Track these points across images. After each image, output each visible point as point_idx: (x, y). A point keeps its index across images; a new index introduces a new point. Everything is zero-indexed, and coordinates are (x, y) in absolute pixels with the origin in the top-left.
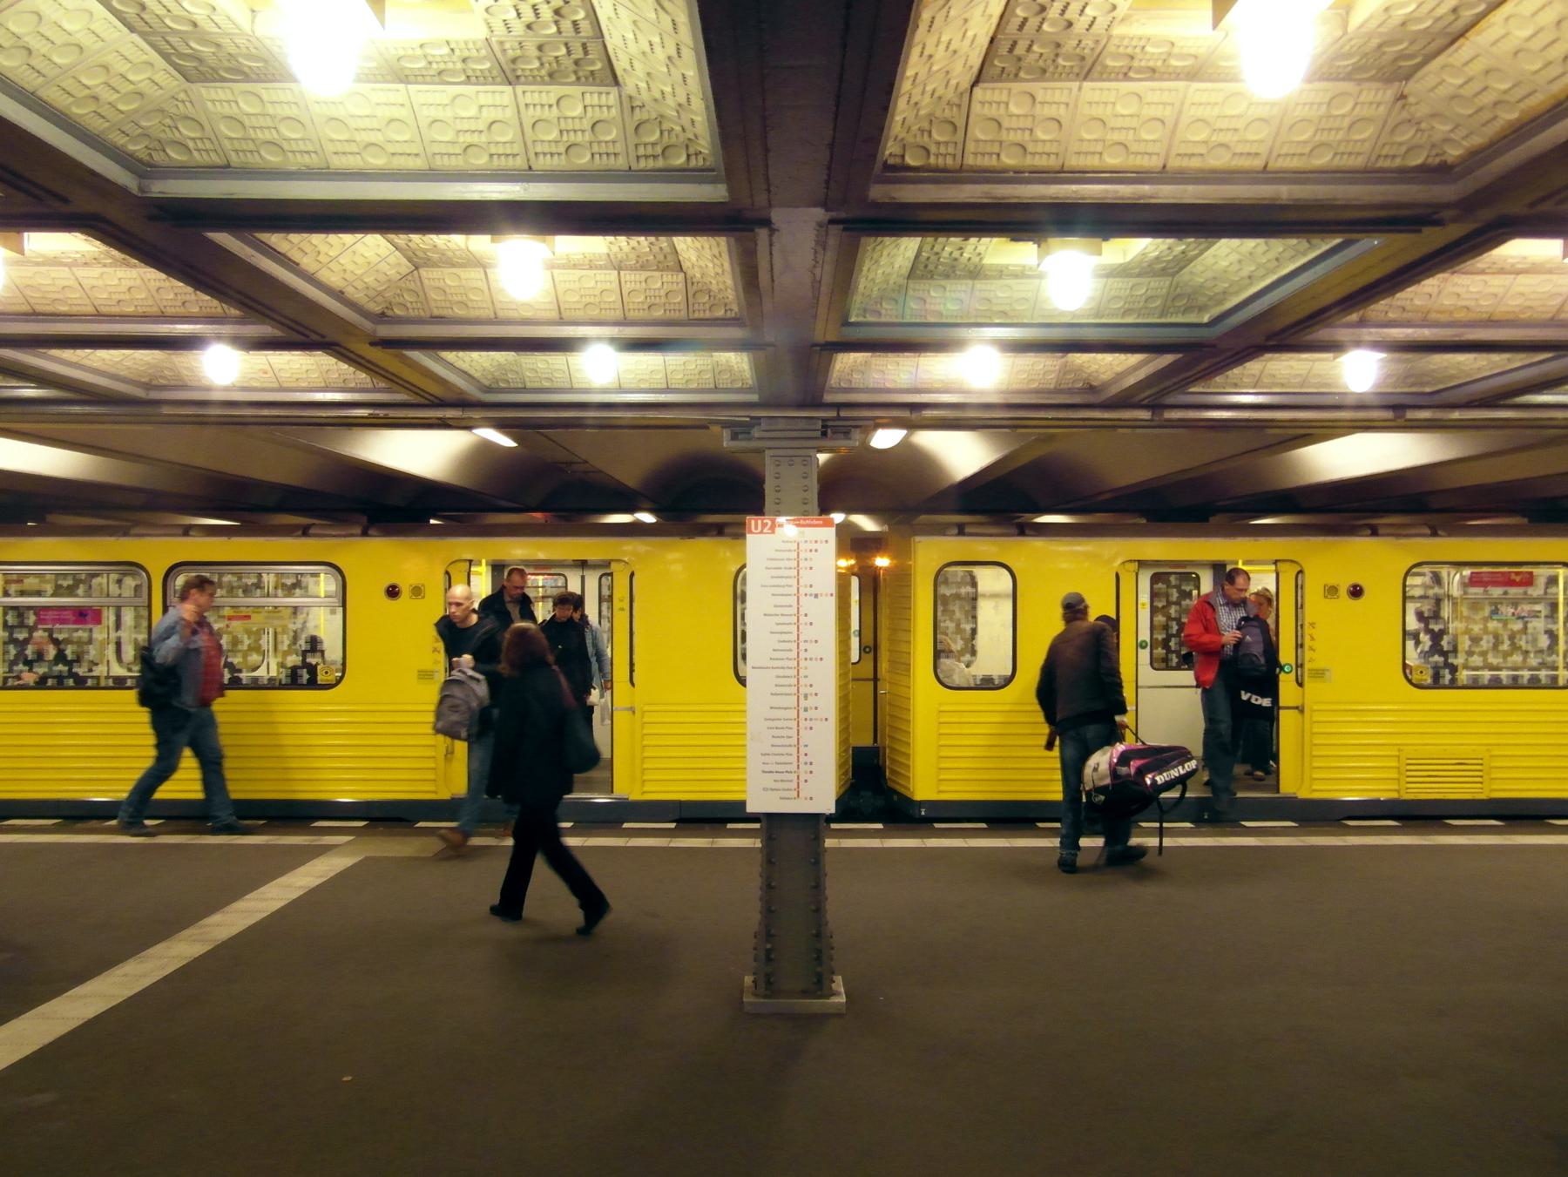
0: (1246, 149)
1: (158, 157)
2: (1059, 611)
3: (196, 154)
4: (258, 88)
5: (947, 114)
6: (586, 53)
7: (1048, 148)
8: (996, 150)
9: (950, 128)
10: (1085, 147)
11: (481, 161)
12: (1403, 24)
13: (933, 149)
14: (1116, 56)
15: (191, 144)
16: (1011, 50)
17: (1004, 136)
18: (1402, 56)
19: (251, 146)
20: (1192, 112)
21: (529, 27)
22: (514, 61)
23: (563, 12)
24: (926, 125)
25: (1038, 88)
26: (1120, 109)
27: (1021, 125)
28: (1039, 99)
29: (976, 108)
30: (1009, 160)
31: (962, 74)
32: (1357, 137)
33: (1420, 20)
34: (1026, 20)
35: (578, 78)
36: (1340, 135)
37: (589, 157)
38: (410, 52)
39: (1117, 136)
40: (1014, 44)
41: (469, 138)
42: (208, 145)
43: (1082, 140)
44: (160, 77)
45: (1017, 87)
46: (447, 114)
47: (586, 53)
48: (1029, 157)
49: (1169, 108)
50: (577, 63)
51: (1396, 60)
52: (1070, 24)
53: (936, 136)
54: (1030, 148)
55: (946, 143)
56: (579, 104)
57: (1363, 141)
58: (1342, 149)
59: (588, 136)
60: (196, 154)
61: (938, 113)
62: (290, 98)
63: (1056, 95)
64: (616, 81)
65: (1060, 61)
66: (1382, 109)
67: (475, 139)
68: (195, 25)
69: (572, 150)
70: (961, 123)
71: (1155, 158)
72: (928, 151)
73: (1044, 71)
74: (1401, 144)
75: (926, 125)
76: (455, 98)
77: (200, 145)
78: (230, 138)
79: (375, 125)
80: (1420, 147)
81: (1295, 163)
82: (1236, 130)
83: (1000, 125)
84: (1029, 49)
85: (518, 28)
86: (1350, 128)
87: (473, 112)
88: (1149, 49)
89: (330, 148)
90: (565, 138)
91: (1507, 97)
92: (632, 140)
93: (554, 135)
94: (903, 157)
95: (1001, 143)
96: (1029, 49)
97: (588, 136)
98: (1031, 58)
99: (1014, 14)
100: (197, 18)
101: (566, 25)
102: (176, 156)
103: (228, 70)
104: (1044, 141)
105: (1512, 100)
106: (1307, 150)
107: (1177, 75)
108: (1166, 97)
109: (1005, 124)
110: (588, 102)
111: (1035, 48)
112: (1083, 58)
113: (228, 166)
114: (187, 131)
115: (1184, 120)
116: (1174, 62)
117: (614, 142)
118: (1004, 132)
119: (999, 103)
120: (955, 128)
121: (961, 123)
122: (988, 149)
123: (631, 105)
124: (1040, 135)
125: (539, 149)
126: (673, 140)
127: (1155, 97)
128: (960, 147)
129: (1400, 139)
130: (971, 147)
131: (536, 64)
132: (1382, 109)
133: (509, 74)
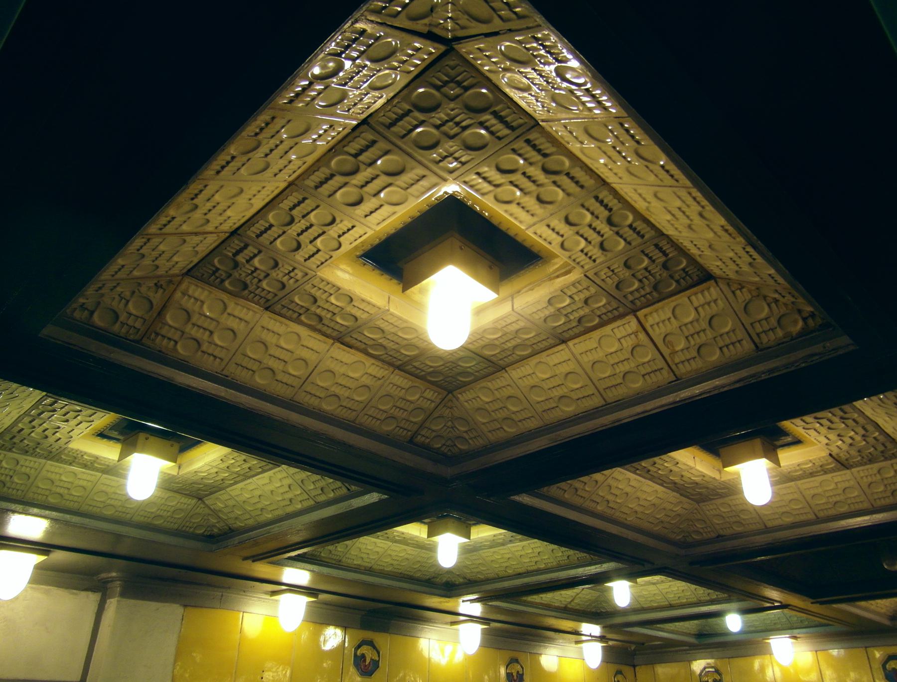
10: (245, 362)
13: (122, 318)
14: (67, 455)
16: (11, 439)
17: (188, 328)
25: (22, 458)
26: (63, 478)
27: (205, 325)
28: (229, 310)
30: (182, 350)
31: (183, 259)
33: (208, 479)
34: (23, 429)
37: (718, 352)
40: (14, 437)
43: (246, 355)
45: (10, 454)
49: (90, 484)
52: (46, 437)
53: (131, 306)
59: (710, 334)
63: (244, 315)
65: (38, 450)
66: (433, 405)
67: (625, 367)
72: (117, 317)
73: (27, 452)
80: (442, 437)
84: (22, 441)
88: (85, 457)
91: (513, 416)
94: (92, 313)
95: (183, 333)
96: (22, 441)
97: (709, 333)
98: (22, 445)
99: (264, 217)
101: (629, 234)
104: (216, 345)
105: (517, 419)
107: (97, 470)
108: (89, 478)
109: (195, 319)
111: (25, 441)
112: (284, 286)
116: (96, 465)
117: (734, 331)
118: (190, 326)
119: (196, 299)
124: (16, 479)
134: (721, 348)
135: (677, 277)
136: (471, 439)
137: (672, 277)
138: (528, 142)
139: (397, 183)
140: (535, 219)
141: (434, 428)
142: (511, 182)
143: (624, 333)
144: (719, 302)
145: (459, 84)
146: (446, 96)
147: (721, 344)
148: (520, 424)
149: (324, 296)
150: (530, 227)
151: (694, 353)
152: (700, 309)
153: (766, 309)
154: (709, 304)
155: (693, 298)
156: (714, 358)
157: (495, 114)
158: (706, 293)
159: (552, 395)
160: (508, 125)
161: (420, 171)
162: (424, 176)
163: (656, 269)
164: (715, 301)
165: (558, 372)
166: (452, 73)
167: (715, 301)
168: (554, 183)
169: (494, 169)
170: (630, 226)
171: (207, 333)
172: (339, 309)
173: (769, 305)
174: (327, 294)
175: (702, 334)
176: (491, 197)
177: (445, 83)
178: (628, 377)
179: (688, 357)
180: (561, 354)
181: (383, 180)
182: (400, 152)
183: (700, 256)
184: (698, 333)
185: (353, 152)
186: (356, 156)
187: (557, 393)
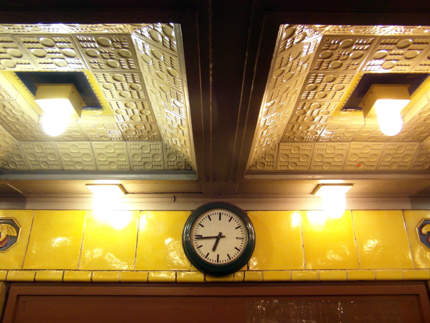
0: (370, 164)
1: (7, 167)
2: (16, 296)
3: (18, 166)
4: (41, 143)
5: (271, 152)
6: (151, 128)
7: (338, 164)
8: (321, 164)
9: (272, 157)
11: (114, 167)
12: (425, 120)
13: (266, 164)
15: (17, 163)
18: (421, 133)
19: (38, 163)
20: (352, 152)
21: (131, 118)
22: (126, 132)
23: (143, 112)
24: (264, 156)
29: (281, 151)
32: (406, 160)
35: (149, 139)
36: (400, 160)
37: (151, 166)
38: (91, 129)
39: (327, 160)
41: (111, 160)
42: (23, 163)
44: (7, 140)
46: (104, 152)
47: (151, 128)
48: (298, 167)
50: (148, 132)
51: (419, 134)
54: (298, 164)
55: (270, 162)
56: (149, 148)
57: (408, 162)
58: (400, 164)
59: (151, 159)
60: (18, 166)
61: (268, 152)
62: (52, 147)
64: (162, 140)
66: (414, 151)
67: (113, 160)
68: (18, 119)
69: (146, 164)
70: (275, 156)
71: (340, 167)
74: (421, 162)
75: (264, 156)
76: (107, 146)
77: (20, 163)
78: (31, 161)
79: (80, 156)
81: (387, 168)
82: (366, 158)
83: (288, 156)
85: (127, 118)
86: (403, 158)
87: (112, 151)
89: (64, 163)
90: (143, 160)
92: (166, 159)
93: (139, 159)
97: (151, 159)
100: (18, 117)
101: (144, 117)
102: (12, 167)
103: (30, 136)
106: (389, 164)
108: (343, 147)
109: (290, 156)
110: (152, 148)
113: (63, 170)
114: (17, 159)
115: (350, 154)
117: (160, 161)
120: (273, 157)
121: (275, 156)
122: (319, 164)
123: (165, 147)
125: (135, 164)
126: (180, 160)
127: (340, 147)
128: (309, 163)
129: (421, 160)
130: (279, 164)
131: (134, 133)
132: (414, 151)
133: (125, 139)
134: (153, 166)
135: (150, 137)
136: (20, 165)
137: (148, 136)
138: (133, 75)
139: (66, 59)
140: (113, 99)
141: (173, 160)
142: (114, 83)
143: (118, 147)
144: (160, 151)
145: (122, 45)
146: (113, 45)
147: (154, 164)
148: (50, 166)
149: (324, 152)
150: (350, 145)
151: (142, 164)
152: (152, 150)
153: (175, 158)
154: (156, 149)
155: (152, 146)
156: (149, 168)
157: (128, 61)
158: (157, 146)
159: (73, 160)
160: (129, 66)
161: (81, 61)
162: (80, 64)
163: (145, 132)
164: (159, 149)
165: (81, 152)
166: (123, 40)
167: (159, 149)
168: (131, 92)
169: (112, 76)
170: (146, 116)
171: (297, 159)
172: (322, 163)
173: (176, 157)
174: (324, 150)
175: (148, 158)
176: (101, 84)
177: (117, 42)
178: (112, 164)
179: (140, 164)
180: (86, 145)
181: (61, 55)
182: (77, 51)
183: (164, 134)
184: (147, 158)
185: (56, 40)
186: (56, 42)
187: (76, 160)
